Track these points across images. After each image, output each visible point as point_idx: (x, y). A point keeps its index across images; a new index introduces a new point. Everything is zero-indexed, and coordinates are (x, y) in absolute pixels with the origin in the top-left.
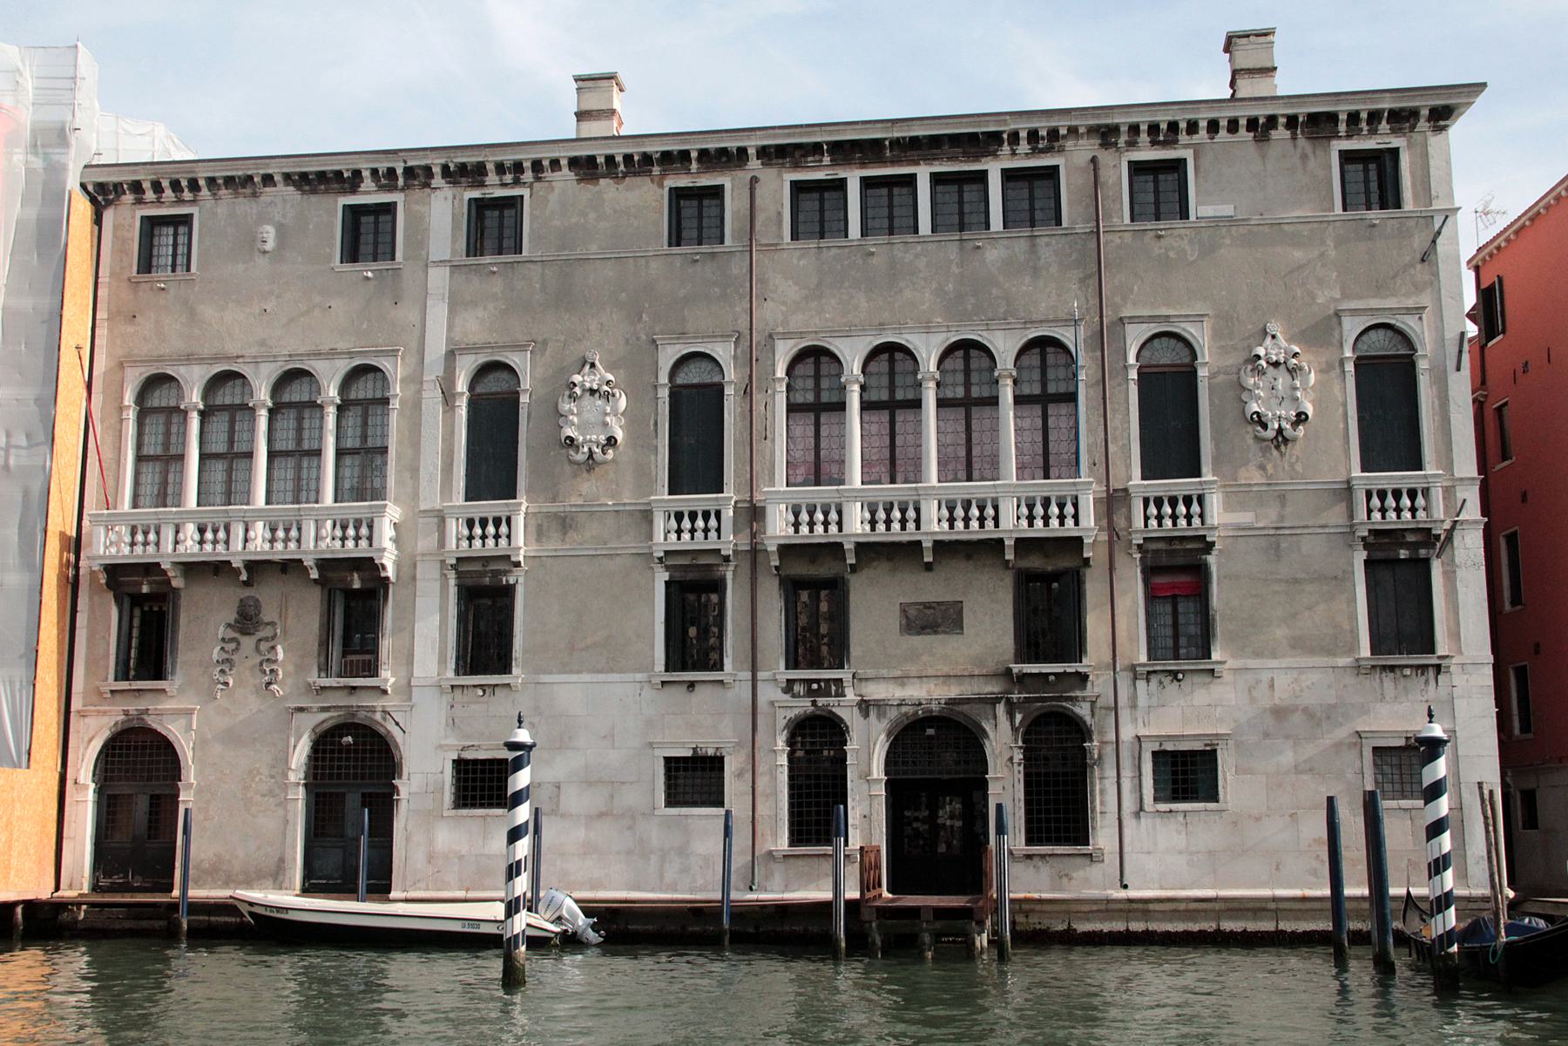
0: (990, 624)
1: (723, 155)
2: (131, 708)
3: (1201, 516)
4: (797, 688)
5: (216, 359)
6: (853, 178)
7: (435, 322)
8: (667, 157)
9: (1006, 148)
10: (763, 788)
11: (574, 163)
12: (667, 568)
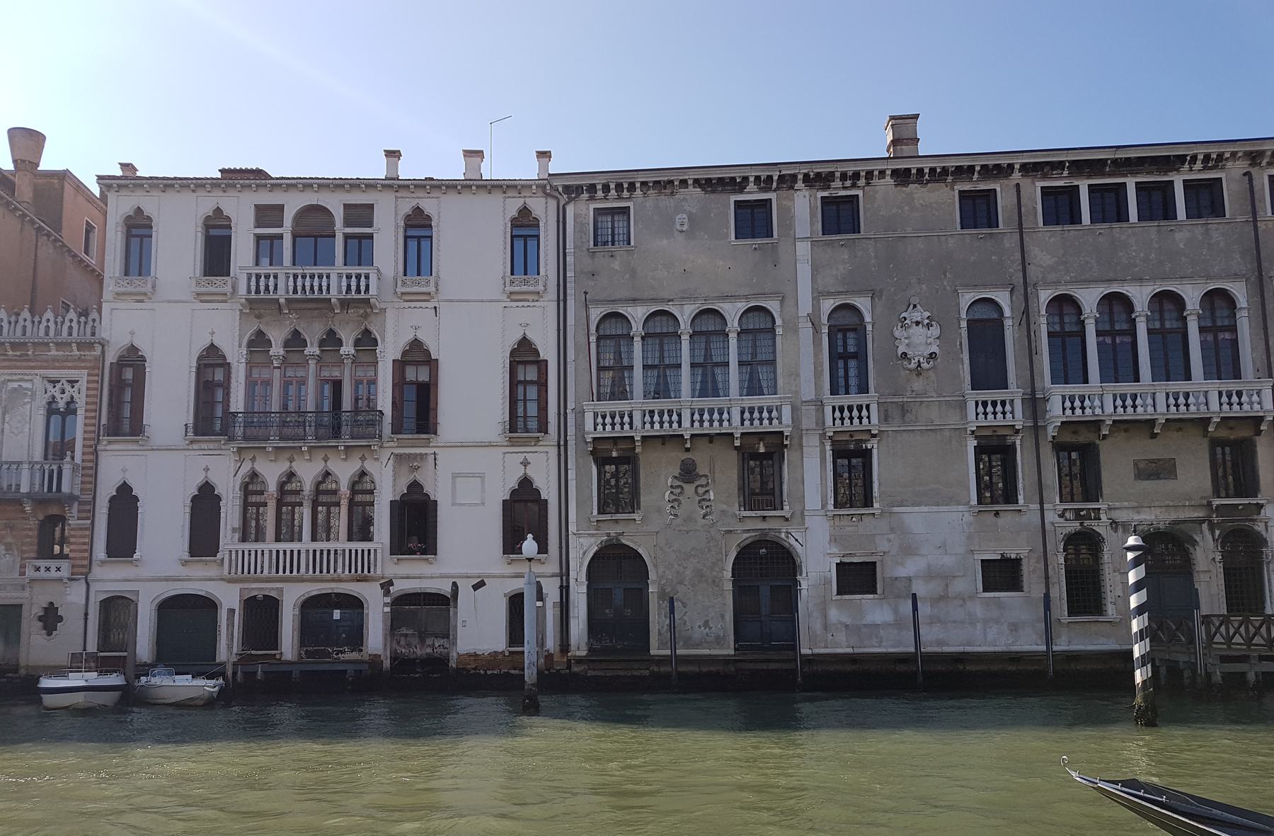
0: (1195, 475)
1: (997, 169)
2: (613, 533)
3: (868, 417)
4: (1067, 515)
5: (654, 300)
6: (1083, 185)
7: (805, 280)
8: (959, 169)
9: (1187, 166)
10: (1047, 577)
11: (895, 173)
12: (976, 438)
